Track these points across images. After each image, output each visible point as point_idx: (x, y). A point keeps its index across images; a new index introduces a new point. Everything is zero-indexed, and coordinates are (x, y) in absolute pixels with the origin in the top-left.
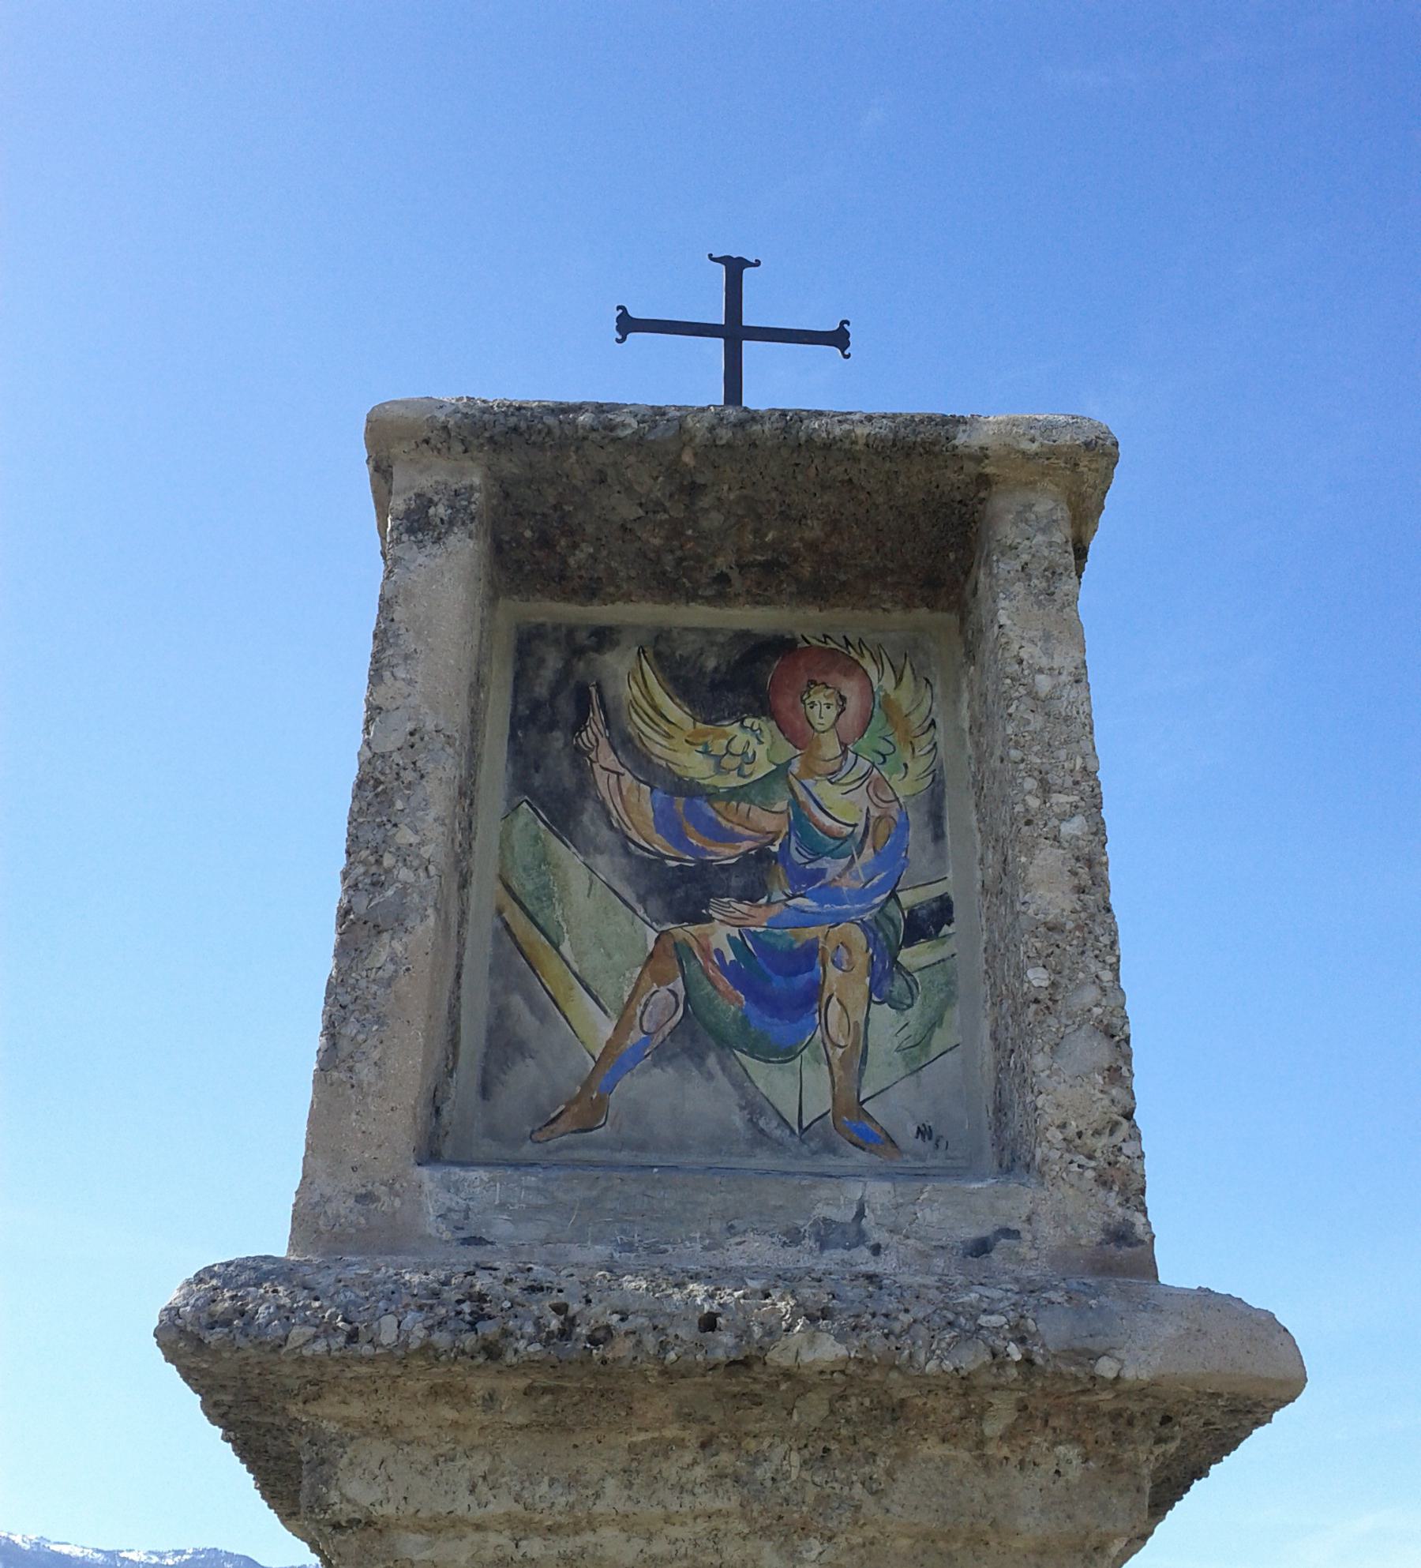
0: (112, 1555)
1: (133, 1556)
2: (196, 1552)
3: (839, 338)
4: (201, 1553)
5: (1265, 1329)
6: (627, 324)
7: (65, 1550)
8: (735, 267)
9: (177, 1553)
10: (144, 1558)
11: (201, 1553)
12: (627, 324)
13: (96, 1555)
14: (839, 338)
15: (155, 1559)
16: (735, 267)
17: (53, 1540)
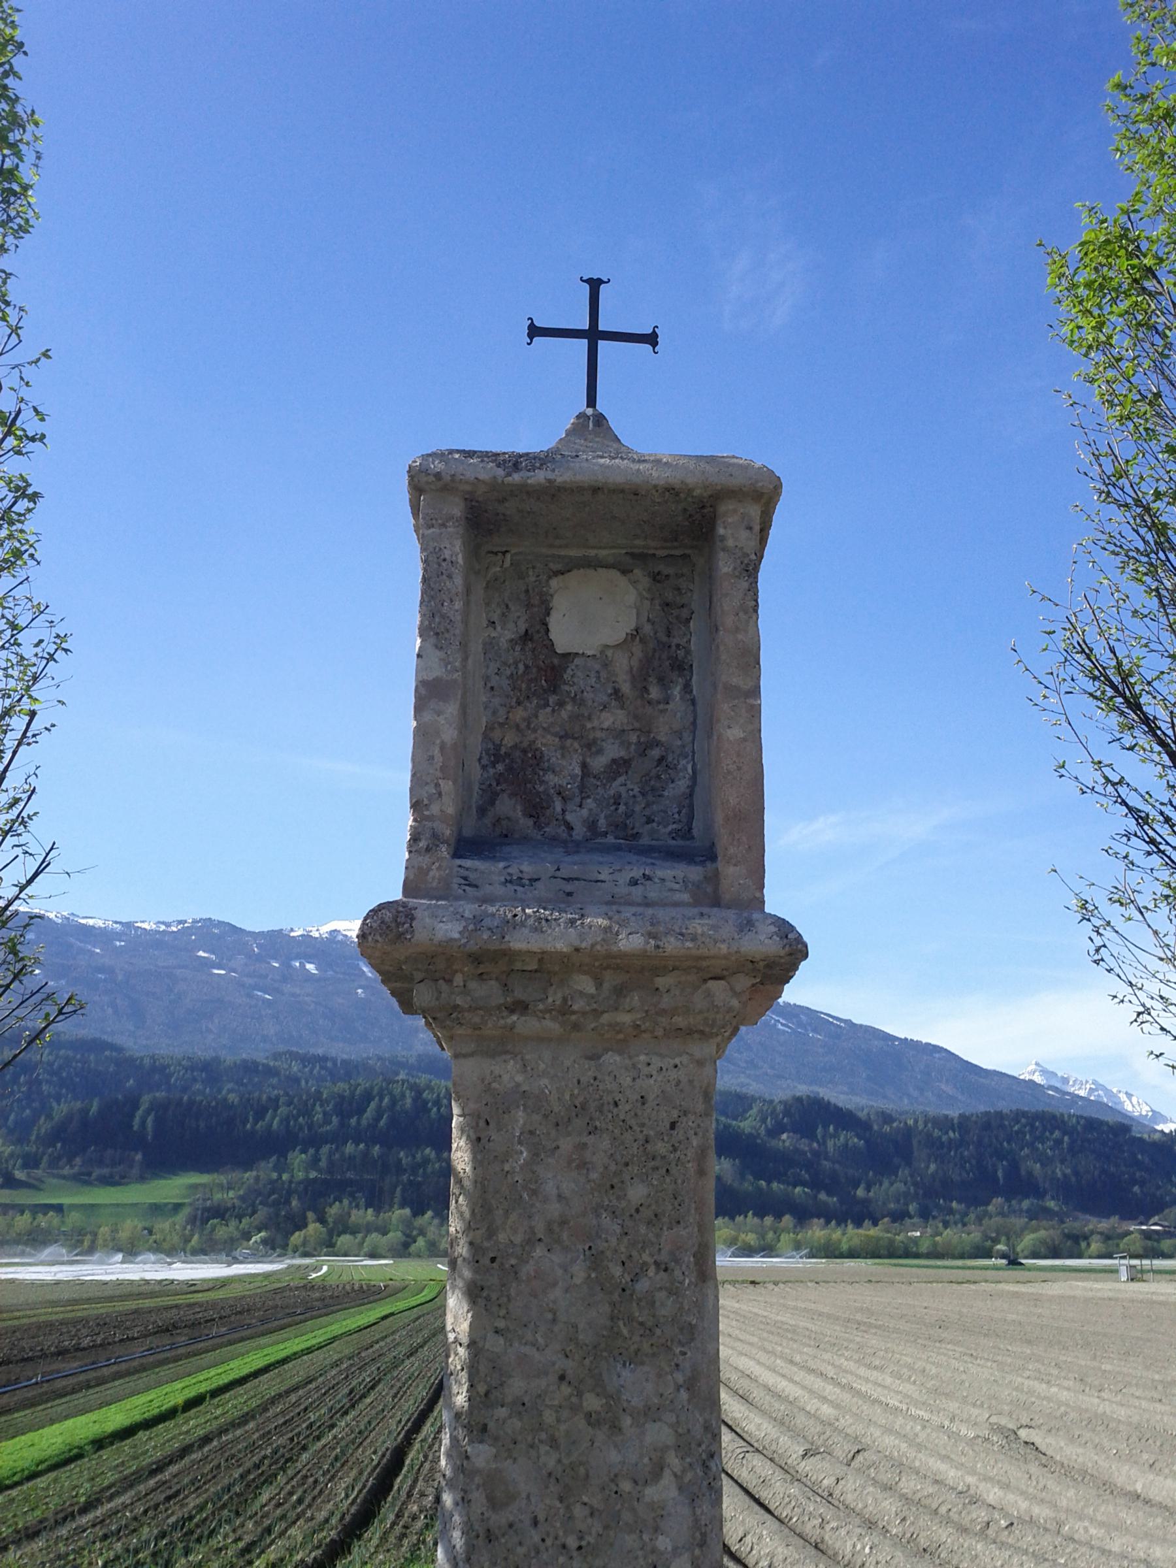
1: (145, 926)
2: (195, 921)
3: (651, 339)
6: (534, 331)
7: (91, 922)
9: (180, 922)
12: (534, 331)
15: (163, 927)
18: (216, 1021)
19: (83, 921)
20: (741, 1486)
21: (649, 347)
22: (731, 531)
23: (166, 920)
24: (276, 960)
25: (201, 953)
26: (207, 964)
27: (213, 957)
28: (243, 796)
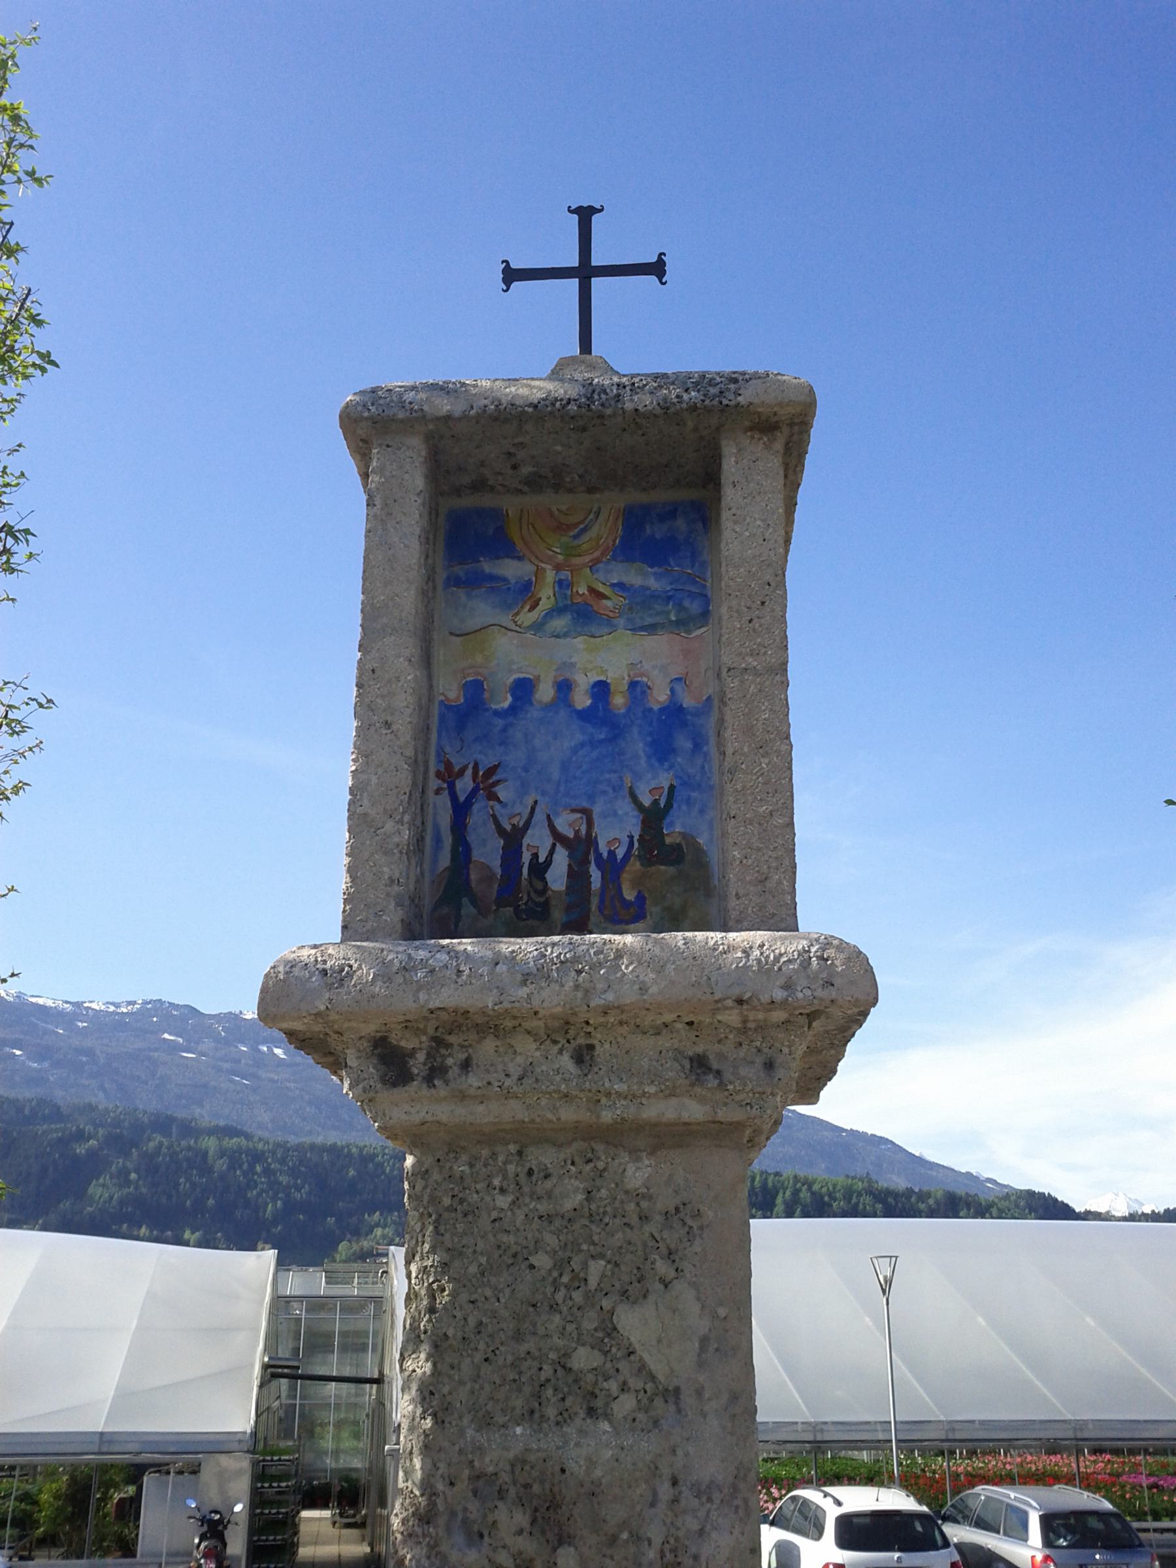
0: (78, 1005)
1: (94, 1006)
2: (145, 1003)
3: (657, 269)
4: (149, 1003)
5: (858, 961)
6: (511, 275)
7: (41, 1001)
8: (585, 215)
9: (130, 1003)
10: (103, 1007)
11: (149, 1003)
12: (511, 275)
13: (66, 1006)
14: (657, 269)
15: (112, 1008)
16: (585, 215)
17: (29, 994)
18: (208, 1107)
19: (33, 1000)
20: (1154, 1217)
21: (653, 279)
22: (744, 467)
23: (117, 1001)
24: (243, 1042)
25: (166, 1036)
26: (174, 1048)
27: (181, 1040)
28: (187, 845)
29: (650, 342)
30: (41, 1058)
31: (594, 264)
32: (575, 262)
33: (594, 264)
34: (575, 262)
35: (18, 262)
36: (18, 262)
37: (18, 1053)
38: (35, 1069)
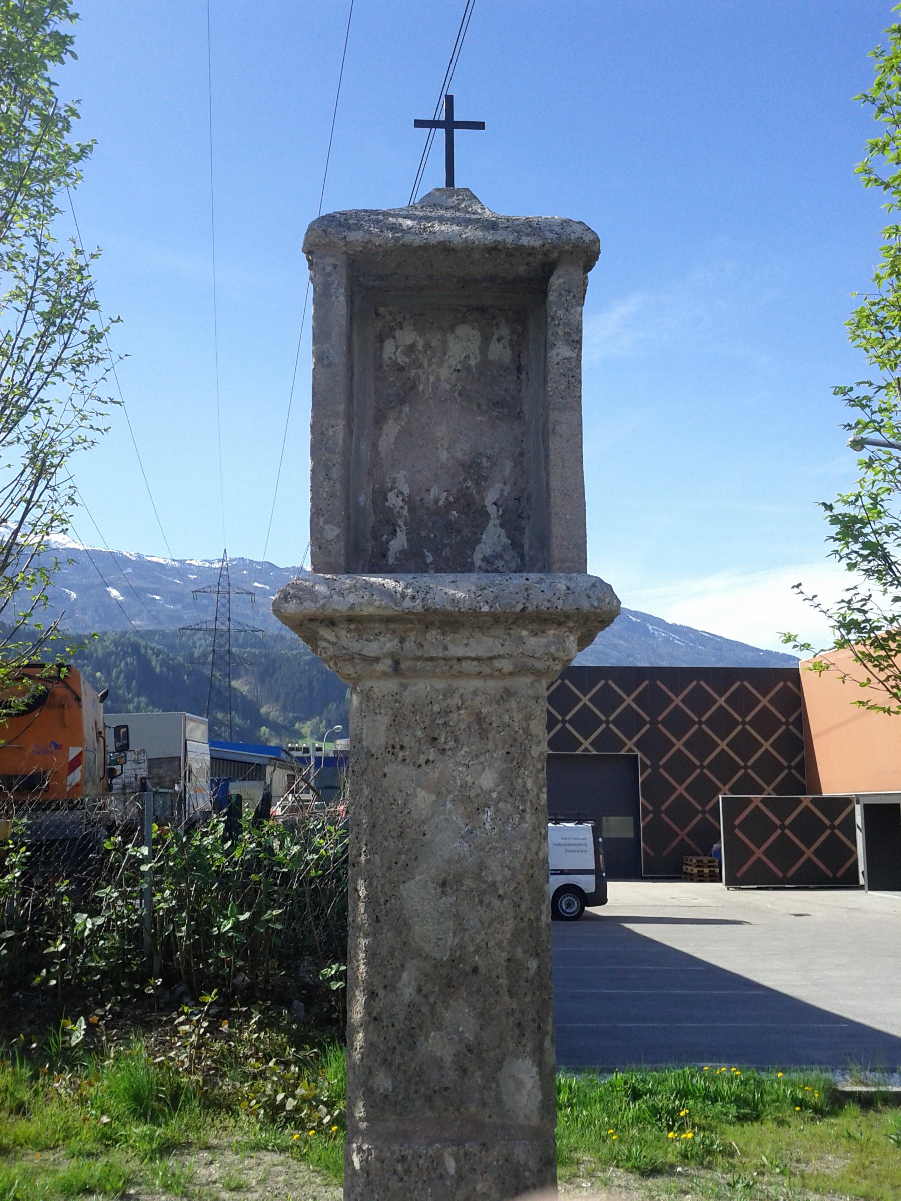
1: (193, 563)
7: (155, 560)
10: (201, 564)
15: (207, 565)
23: (210, 559)
25: (256, 584)
27: (268, 588)
29: (512, 188)
30: (174, 602)
31: (455, 119)
32: (456, 131)
33: (455, 119)
34: (456, 131)
35: (74, 56)
36: (74, 56)
37: (158, 598)
38: (171, 609)
